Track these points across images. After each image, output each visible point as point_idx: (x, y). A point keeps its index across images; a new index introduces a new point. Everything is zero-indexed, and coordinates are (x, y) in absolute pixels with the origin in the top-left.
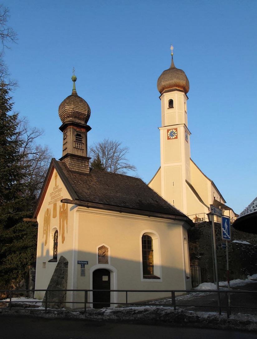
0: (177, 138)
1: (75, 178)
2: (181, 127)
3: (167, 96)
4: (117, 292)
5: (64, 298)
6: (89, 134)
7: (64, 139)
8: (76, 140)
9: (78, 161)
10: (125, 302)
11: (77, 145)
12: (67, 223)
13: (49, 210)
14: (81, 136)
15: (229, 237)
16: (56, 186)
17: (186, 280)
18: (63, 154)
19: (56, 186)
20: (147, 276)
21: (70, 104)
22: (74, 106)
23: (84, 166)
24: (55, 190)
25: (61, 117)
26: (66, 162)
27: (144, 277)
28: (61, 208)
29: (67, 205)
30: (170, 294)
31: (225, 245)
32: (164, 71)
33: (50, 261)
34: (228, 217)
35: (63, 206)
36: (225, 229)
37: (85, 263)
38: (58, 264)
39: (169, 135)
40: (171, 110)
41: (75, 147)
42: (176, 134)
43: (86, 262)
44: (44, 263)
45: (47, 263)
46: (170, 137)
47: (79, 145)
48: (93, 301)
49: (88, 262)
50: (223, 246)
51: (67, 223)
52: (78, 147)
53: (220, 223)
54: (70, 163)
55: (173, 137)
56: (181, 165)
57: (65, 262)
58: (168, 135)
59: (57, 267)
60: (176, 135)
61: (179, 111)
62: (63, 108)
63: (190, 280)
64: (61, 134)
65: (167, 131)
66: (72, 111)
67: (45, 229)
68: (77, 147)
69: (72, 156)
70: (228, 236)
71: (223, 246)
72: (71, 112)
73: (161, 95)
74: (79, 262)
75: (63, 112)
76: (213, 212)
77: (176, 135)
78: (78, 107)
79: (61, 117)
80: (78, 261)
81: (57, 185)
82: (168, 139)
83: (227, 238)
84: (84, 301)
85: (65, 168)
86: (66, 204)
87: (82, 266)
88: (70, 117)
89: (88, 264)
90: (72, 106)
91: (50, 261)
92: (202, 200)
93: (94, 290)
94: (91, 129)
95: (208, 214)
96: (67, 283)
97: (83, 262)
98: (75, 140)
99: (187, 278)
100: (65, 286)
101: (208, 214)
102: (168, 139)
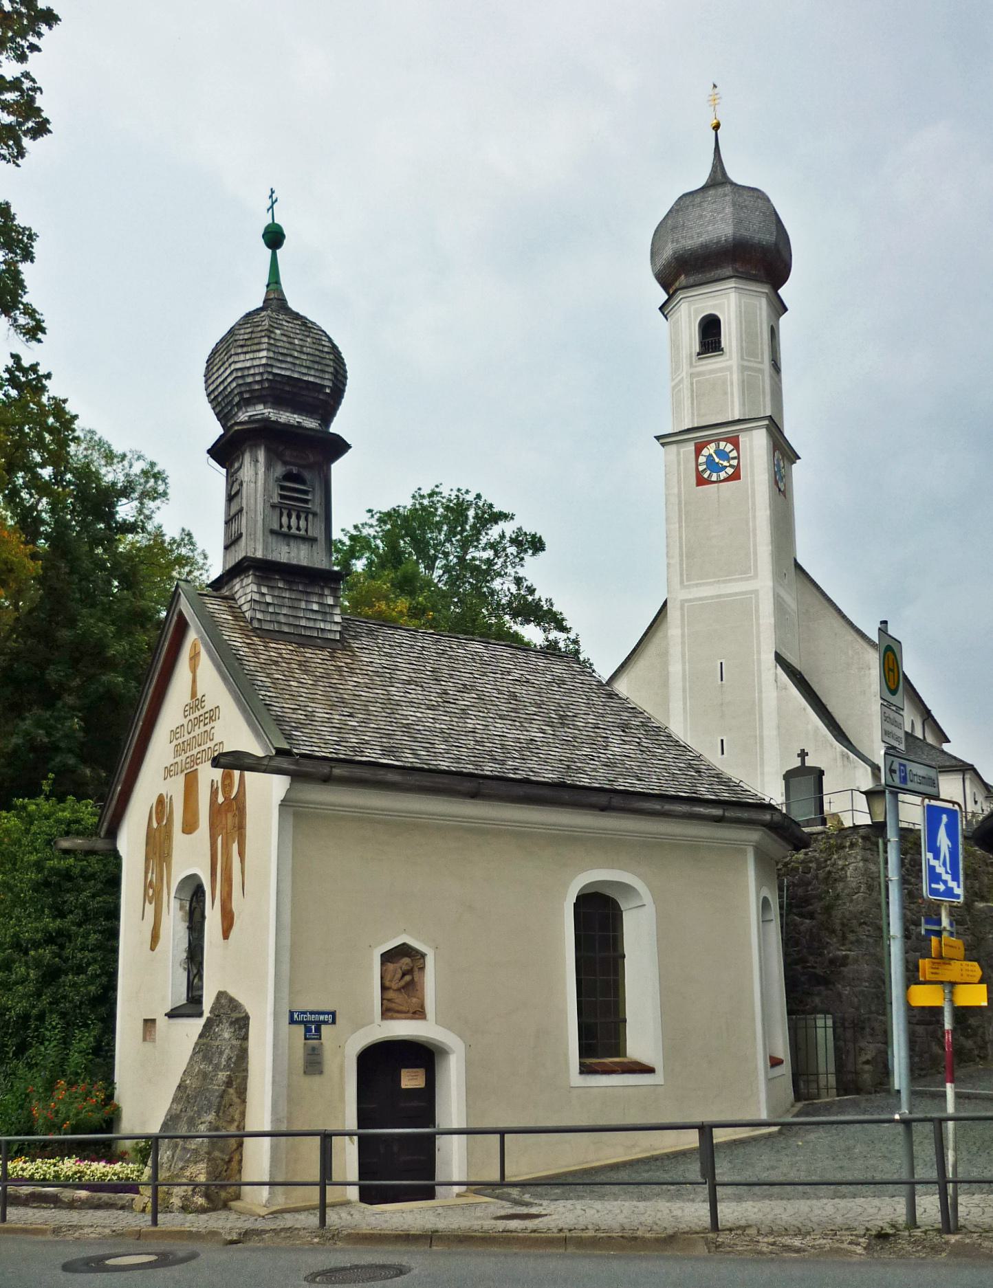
1: (276, 663)
2: (755, 432)
3: (693, 308)
4: (465, 1136)
5: (234, 1164)
6: (339, 469)
7: (230, 498)
8: (282, 497)
9: (290, 590)
11: (285, 520)
12: (241, 854)
13: (167, 801)
14: (303, 482)
15: (959, 891)
16: (196, 701)
17: (766, 1072)
18: (225, 562)
19: (196, 701)
20: (595, 1064)
21: (255, 348)
22: (271, 355)
23: (315, 607)
24: (192, 717)
25: (215, 403)
26: (237, 596)
27: (585, 1070)
28: (214, 793)
29: (242, 780)
30: (691, 1139)
31: (939, 922)
32: (680, 198)
33: (173, 1014)
34: (954, 803)
35: (227, 779)
36: (937, 857)
37: (322, 1018)
38: (205, 1026)
39: (701, 468)
40: (713, 363)
41: (276, 527)
43: (328, 1013)
44: (146, 1021)
45: (162, 1022)
46: (706, 476)
47: (294, 520)
48: (362, 1175)
49: (333, 1014)
50: (929, 927)
51: (241, 854)
52: (289, 527)
53: (917, 827)
54: (256, 597)
55: (723, 475)
56: (756, 592)
57: (235, 1015)
58: (697, 465)
59: (201, 1036)
60: (731, 466)
61: (746, 363)
62: (227, 365)
63: (786, 1069)
64: (217, 474)
65: (693, 448)
66: (265, 376)
67: (151, 881)
68: (285, 529)
69: (265, 570)
70: (952, 884)
71: (929, 927)
72: (258, 378)
73: (666, 297)
74: (296, 1016)
75: (222, 382)
76: (897, 782)
77: (731, 466)
78: (289, 359)
79: (215, 403)
80: (292, 1013)
81: (199, 696)
82: (701, 481)
83: (949, 892)
84: (317, 1178)
85: (236, 618)
86: (237, 773)
87: (308, 1030)
88: (255, 401)
89: (334, 1022)
90: (264, 353)
91: (173, 1014)
92: (844, 733)
93: (361, 1131)
95: (868, 794)
96: (244, 1101)
97: (312, 1013)
98: (276, 500)
99: (775, 1062)
100: (237, 1117)
101: (868, 794)
102: (701, 481)
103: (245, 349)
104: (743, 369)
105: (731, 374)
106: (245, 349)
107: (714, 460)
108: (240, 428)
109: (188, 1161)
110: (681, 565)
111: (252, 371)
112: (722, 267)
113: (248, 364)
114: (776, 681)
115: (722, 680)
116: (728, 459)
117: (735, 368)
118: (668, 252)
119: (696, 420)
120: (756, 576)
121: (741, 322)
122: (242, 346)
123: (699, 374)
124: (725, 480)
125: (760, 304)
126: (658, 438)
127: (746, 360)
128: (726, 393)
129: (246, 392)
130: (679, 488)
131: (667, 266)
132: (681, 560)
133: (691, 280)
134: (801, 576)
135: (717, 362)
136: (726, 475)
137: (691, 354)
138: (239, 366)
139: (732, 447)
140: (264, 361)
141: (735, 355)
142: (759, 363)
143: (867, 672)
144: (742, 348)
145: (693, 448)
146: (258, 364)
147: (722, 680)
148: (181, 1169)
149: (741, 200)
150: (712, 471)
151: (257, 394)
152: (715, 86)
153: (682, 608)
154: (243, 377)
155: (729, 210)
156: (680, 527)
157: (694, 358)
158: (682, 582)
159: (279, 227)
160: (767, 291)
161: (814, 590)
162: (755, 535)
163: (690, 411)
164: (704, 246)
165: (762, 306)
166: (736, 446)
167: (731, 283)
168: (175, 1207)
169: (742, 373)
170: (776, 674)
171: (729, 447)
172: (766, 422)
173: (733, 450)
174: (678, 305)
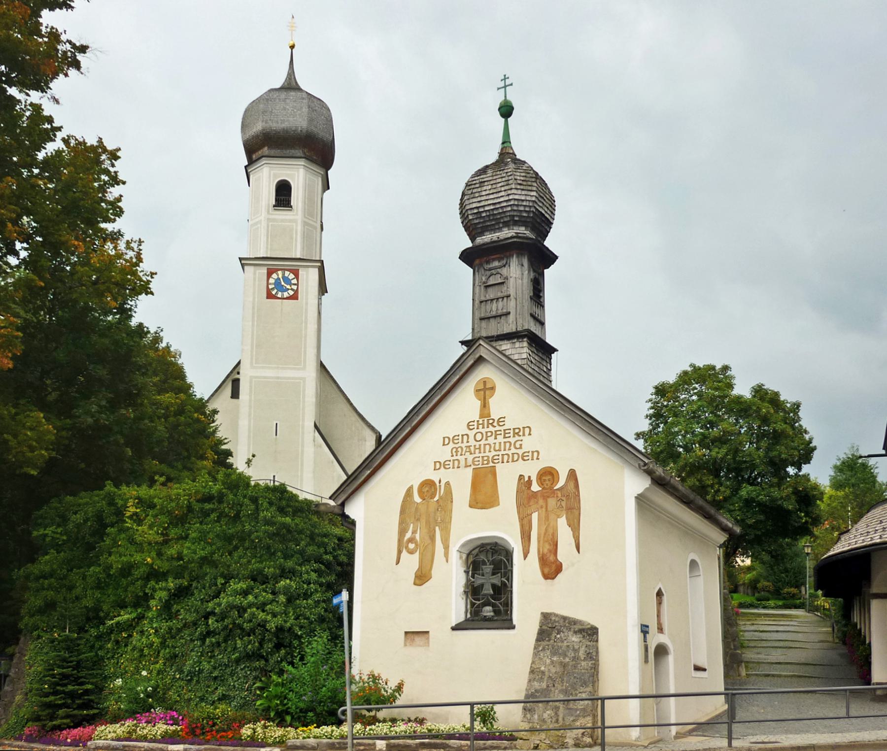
0: (297, 298)
2: (311, 269)
10: (606, 724)
27: (297, 299)
30: (853, 713)
40: (283, 215)
42: (295, 287)
55: (286, 295)
56: (304, 379)
58: (268, 284)
60: (292, 289)
61: (306, 220)
72: (527, 209)
77: (292, 289)
82: (270, 296)
94: (556, 257)
102: (270, 296)
103: (522, 187)
104: (305, 224)
105: (297, 226)
106: (522, 187)
107: (280, 283)
108: (518, 240)
109: (579, 716)
110: (252, 352)
111: (524, 203)
112: (295, 149)
113: (523, 198)
114: (314, 441)
115: (276, 435)
116: (291, 284)
117: (299, 222)
118: (258, 127)
119: (269, 252)
120: (304, 368)
121: (305, 190)
122: (520, 184)
123: (274, 220)
124: (287, 298)
125: (318, 181)
126: (240, 259)
127: (306, 218)
128: (291, 238)
129: (517, 216)
130: (254, 298)
131: (256, 137)
132: (252, 348)
133: (273, 152)
134: (325, 373)
135: (279, 215)
136: (288, 295)
137: (269, 205)
138: (516, 197)
139: (294, 277)
140: (534, 199)
141: (300, 213)
142: (314, 222)
143: (364, 443)
144: (305, 209)
145: (266, 271)
146: (530, 199)
147: (276, 435)
148: (573, 721)
149: (312, 105)
150: (278, 290)
151: (523, 219)
152: (293, 17)
153: (251, 382)
154: (517, 205)
155: (305, 110)
156: (253, 325)
157: (271, 207)
158: (251, 363)
159: (510, 102)
160: (322, 173)
161: (331, 382)
162: (305, 340)
163: (265, 246)
164: (286, 131)
165: (319, 182)
166: (297, 276)
167: (302, 162)
168: (569, 745)
169: (304, 226)
170: (314, 436)
171: (292, 276)
172: (319, 264)
173: (294, 278)
174: (262, 167)
